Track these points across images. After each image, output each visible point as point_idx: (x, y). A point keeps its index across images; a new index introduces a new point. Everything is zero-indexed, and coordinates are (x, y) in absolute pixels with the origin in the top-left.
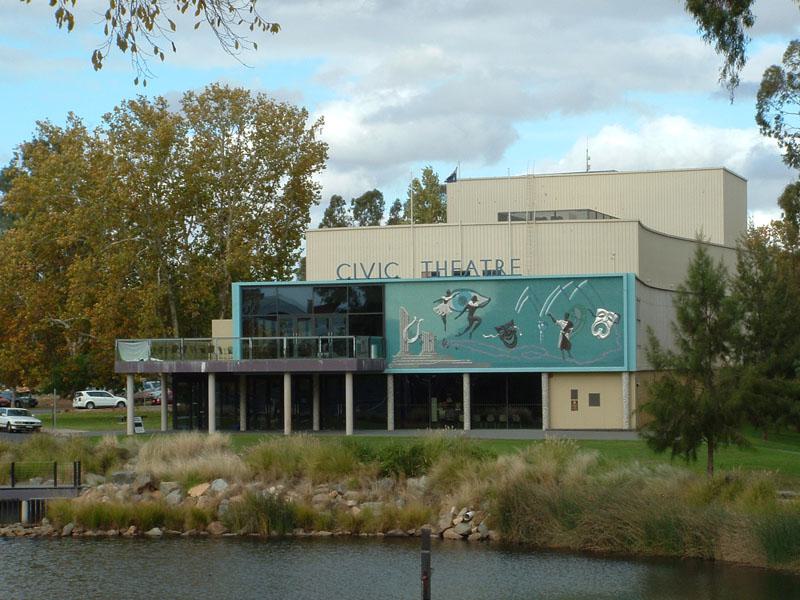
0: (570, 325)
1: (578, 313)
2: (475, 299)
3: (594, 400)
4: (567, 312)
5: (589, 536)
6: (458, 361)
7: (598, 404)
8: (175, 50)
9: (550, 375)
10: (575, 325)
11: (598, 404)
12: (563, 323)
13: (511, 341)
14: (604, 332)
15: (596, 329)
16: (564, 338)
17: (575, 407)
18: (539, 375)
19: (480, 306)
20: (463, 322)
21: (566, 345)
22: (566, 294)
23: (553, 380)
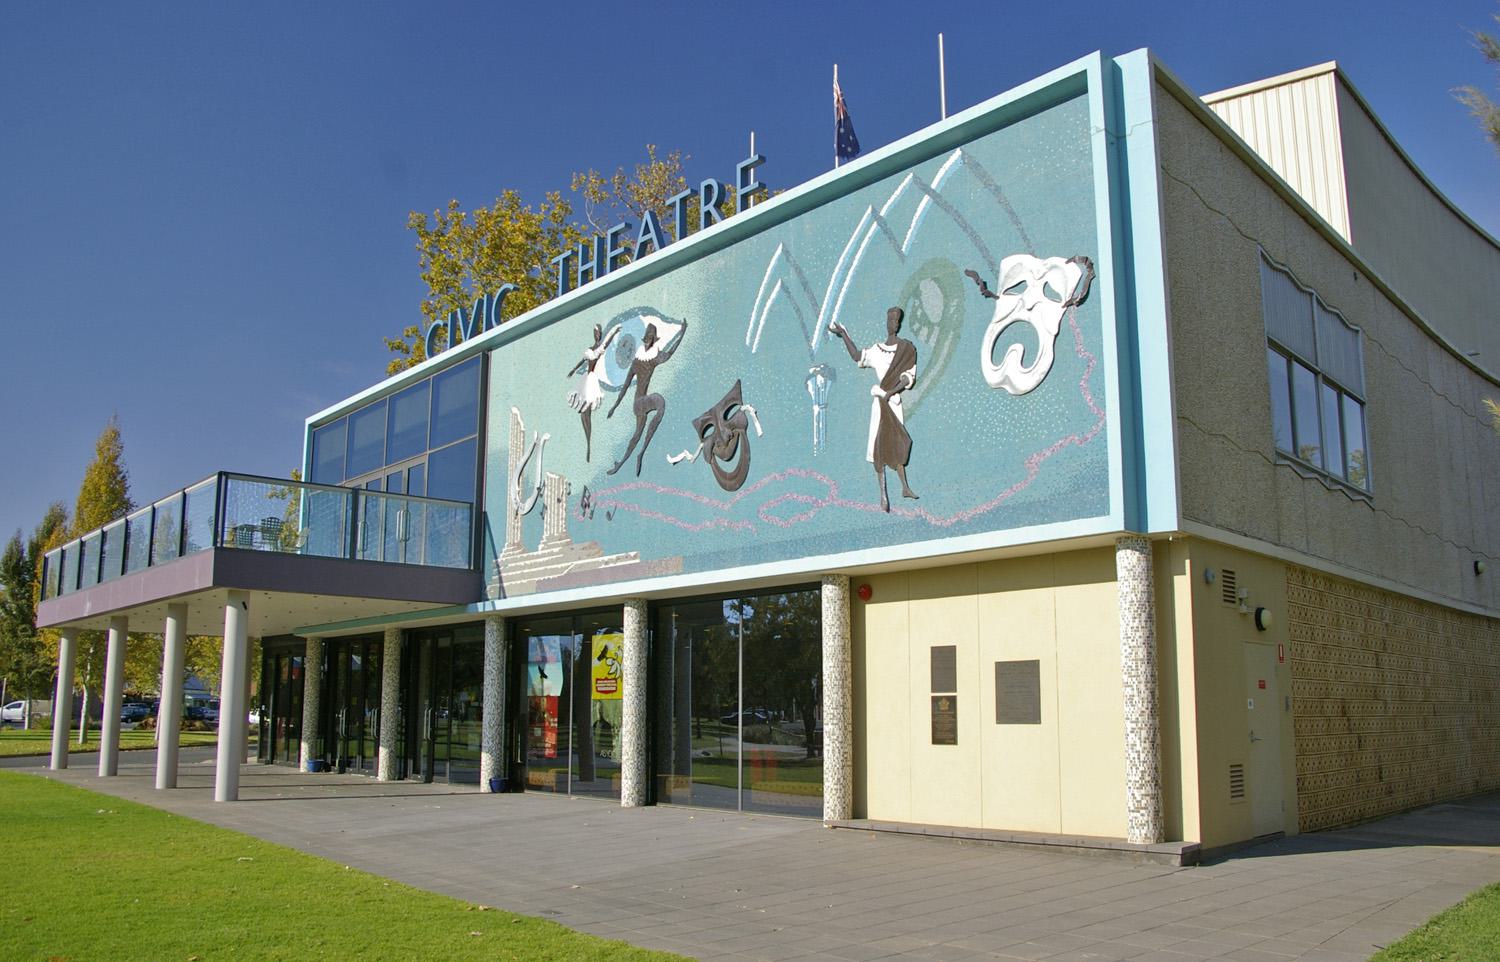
0: (906, 356)
1: (932, 301)
2: (651, 337)
3: (1019, 692)
4: (896, 303)
5: (134, 943)
6: (604, 561)
7: (1032, 715)
8: (610, 416)
9: (861, 588)
10: (923, 357)
11: (1032, 715)
12: (879, 358)
13: (729, 467)
14: (1026, 360)
15: (997, 355)
16: (887, 413)
17: (944, 731)
18: (807, 588)
19: (665, 356)
20: (624, 423)
21: (894, 446)
22: (889, 232)
23: (873, 612)
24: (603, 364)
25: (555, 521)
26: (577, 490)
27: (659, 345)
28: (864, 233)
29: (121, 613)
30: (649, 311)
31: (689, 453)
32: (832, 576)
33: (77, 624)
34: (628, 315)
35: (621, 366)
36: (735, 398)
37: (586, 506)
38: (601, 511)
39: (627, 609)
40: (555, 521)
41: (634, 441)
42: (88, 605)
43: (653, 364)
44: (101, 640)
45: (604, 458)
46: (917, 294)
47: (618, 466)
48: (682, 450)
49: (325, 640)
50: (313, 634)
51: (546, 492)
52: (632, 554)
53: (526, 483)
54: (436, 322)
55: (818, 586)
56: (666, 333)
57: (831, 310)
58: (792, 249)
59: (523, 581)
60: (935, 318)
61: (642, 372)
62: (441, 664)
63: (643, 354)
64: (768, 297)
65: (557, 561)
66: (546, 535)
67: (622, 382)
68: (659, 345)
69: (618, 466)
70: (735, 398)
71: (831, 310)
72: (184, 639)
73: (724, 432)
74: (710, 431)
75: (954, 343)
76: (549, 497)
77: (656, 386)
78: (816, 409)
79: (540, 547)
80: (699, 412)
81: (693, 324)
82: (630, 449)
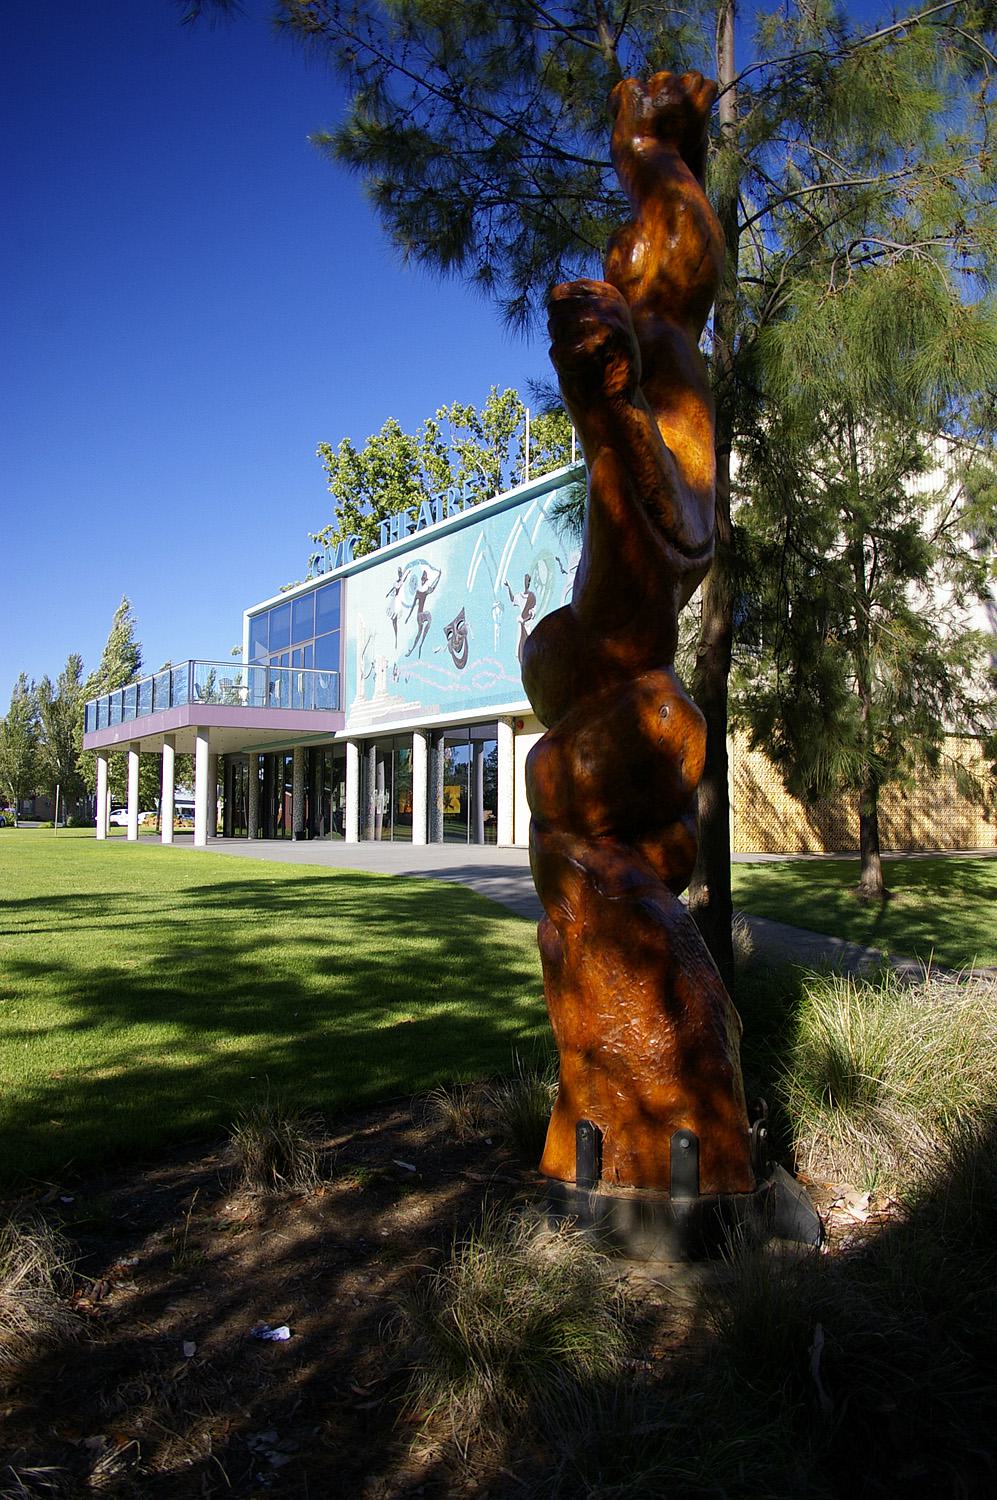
2: (424, 579)
19: (432, 589)
24: (358, 647)
25: (381, 682)
26: (391, 665)
27: (429, 584)
28: (516, 531)
29: (137, 740)
30: (424, 562)
31: (442, 643)
32: (502, 718)
33: (109, 748)
34: (414, 563)
35: (413, 594)
36: (461, 618)
37: (395, 675)
38: (402, 677)
39: (501, 725)
40: (381, 682)
41: (418, 638)
42: (117, 735)
43: (426, 594)
44: (124, 760)
45: (404, 647)
46: (537, 567)
47: (410, 652)
48: (438, 641)
49: (305, 748)
50: (253, 751)
51: (376, 665)
52: (417, 703)
53: (366, 659)
54: (397, 116)
55: (411, 734)
56: (432, 576)
57: (502, 576)
58: (487, 534)
59: (361, 718)
60: (544, 582)
61: (421, 597)
62: (321, 763)
63: (423, 589)
64: (476, 561)
65: (383, 706)
66: (376, 691)
67: (412, 603)
68: (429, 584)
69: (410, 652)
70: (461, 618)
71: (502, 576)
72: (178, 758)
73: (457, 635)
74: (451, 635)
75: (551, 596)
76: (377, 670)
77: (427, 608)
78: (496, 625)
79: (374, 697)
80: (446, 624)
81: (444, 572)
82: (416, 643)
